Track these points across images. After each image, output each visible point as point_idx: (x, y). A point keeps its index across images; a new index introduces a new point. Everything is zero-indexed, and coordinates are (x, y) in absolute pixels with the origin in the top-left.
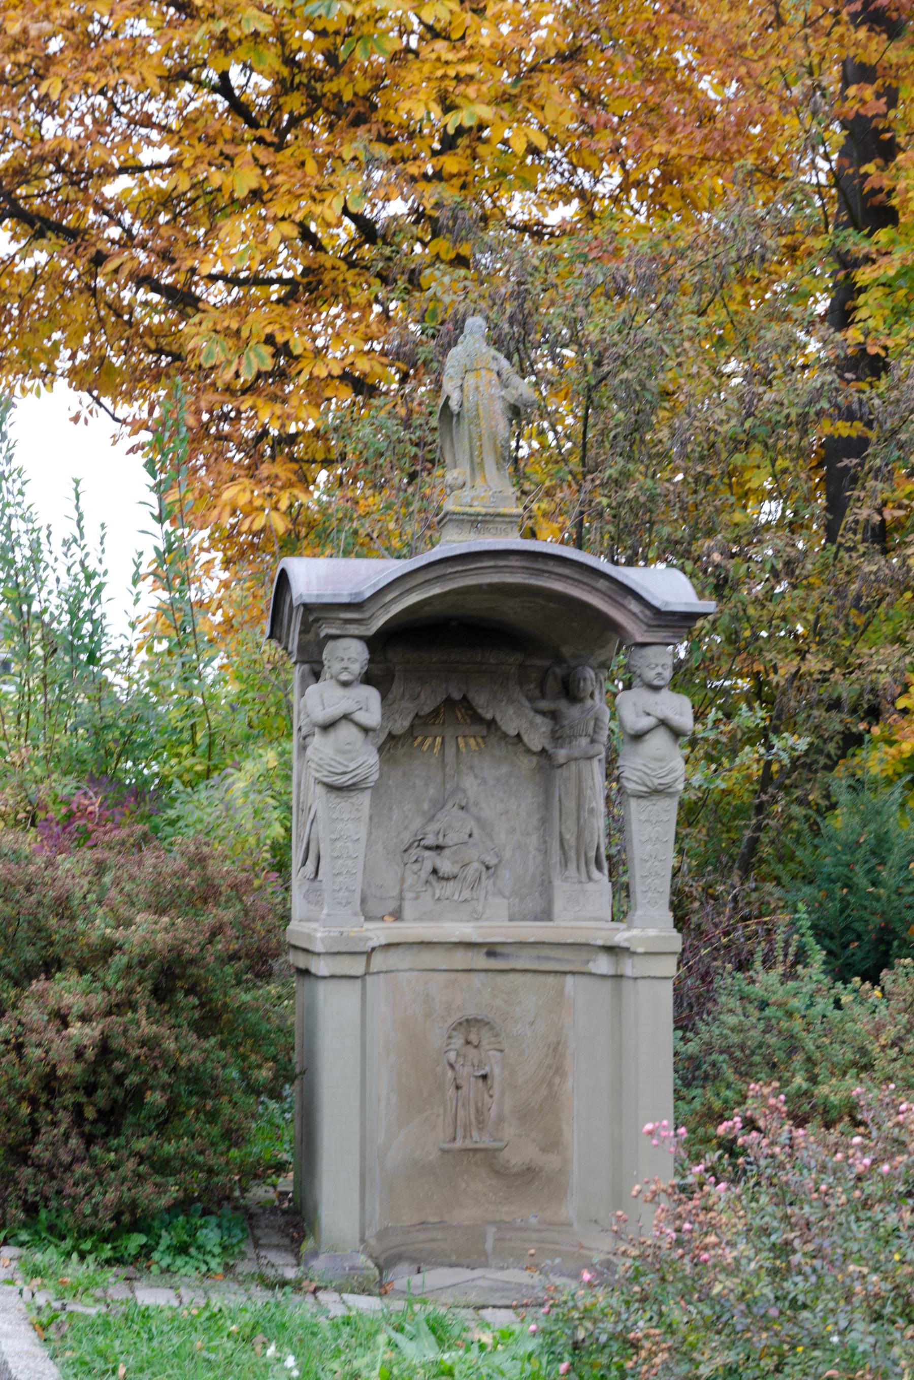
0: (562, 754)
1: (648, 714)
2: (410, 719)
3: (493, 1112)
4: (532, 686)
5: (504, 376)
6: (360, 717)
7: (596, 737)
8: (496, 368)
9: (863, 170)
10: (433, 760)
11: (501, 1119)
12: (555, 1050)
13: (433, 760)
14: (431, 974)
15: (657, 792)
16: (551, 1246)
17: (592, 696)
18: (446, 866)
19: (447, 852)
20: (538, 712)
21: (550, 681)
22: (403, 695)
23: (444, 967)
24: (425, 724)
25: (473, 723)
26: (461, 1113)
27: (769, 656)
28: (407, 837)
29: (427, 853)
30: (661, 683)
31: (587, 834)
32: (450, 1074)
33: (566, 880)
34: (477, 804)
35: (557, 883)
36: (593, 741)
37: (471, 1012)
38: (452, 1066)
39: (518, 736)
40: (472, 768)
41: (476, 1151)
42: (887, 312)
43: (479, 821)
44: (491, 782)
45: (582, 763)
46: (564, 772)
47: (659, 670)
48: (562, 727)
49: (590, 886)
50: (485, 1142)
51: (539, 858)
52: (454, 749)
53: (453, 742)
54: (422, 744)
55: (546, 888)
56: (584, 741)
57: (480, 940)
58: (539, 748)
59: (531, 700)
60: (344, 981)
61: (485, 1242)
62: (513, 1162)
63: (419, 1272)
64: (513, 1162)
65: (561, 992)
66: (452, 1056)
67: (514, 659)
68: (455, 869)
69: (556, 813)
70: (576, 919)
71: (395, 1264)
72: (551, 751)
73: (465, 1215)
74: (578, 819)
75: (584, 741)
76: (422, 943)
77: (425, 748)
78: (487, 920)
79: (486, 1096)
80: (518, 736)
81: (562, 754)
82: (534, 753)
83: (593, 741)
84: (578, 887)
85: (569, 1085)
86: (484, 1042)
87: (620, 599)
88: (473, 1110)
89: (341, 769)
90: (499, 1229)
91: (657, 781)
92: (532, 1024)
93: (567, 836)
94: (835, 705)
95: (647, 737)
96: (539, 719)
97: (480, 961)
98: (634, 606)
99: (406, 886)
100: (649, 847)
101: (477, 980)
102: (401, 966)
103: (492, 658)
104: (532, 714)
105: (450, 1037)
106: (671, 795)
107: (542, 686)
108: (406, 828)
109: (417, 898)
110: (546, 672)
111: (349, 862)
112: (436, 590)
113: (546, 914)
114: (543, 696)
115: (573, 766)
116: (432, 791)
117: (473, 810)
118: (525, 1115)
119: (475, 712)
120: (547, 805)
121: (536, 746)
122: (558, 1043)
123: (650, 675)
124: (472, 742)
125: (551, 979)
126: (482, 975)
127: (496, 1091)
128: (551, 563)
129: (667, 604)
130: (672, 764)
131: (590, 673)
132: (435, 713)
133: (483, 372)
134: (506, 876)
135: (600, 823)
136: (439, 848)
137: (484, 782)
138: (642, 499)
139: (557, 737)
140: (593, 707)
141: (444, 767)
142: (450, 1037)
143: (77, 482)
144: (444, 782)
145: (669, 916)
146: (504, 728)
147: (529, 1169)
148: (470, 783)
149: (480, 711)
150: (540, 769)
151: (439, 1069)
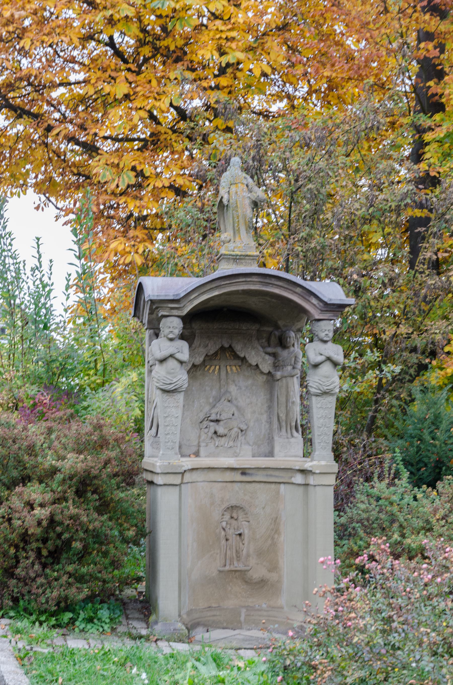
0: (278, 374)
1: (321, 355)
2: (203, 357)
3: (245, 552)
4: (264, 341)
5: (250, 187)
6: (178, 356)
8: (246, 183)
9: (428, 84)
10: (215, 377)
11: (248, 556)
14: (214, 484)
15: (325, 393)
17: (293, 345)
18: (221, 430)
19: (221, 423)
20: (267, 353)
21: (273, 338)
22: (200, 345)
23: (220, 480)
24: (211, 359)
25: (234, 359)
26: (229, 553)
27: (381, 325)
28: (202, 416)
29: (212, 424)
30: (328, 339)
31: (291, 414)
32: (223, 533)
33: (280, 437)
34: (236, 399)
35: (276, 438)
36: (294, 368)
37: (234, 502)
38: (224, 529)
39: (257, 365)
40: (234, 381)
41: (236, 571)
43: (237, 407)
44: (243, 388)
45: (289, 379)
46: (280, 383)
47: (327, 332)
48: (279, 361)
49: (292, 440)
50: (240, 567)
51: (267, 426)
52: (225, 372)
53: (225, 368)
55: (271, 441)
56: (289, 368)
57: (238, 467)
58: (267, 371)
59: (263, 347)
61: (240, 616)
62: (254, 577)
64: (254, 577)
65: (278, 492)
66: (224, 524)
67: (255, 327)
68: (226, 432)
69: (276, 404)
70: (285, 456)
71: (196, 628)
72: (273, 373)
73: (230, 603)
74: (287, 406)
75: (289, 368)
76: (209, 468)
77: (211, 371)
78: (242, 456)
79: (241, 544)
80: (257, 365)
81: (278, 374)
82: (265, 374)
83: (294, 368)
84: (286, 440)
85: (282, 538)
86: (240, 517)
87: (307, 297)
88: (234, 551)
89: (169, 382)
91: (325, 388)
92: (264, 508)
93: (281, 415)
94: (414, 350)
95: (321, 366)
96: (267, 357)
97: (238, 477)
98: (314, 301)
99: (201, 440)
100: (322, 420)
101: (236, 486)
102: (199, 479)
103: (244, 327)
104: (264, 354)
105: (223, 515)
106: (332, 395)
107: (268, 340)
108: (201, 411)
109: (207, 446)
111: (173, 428)
112: (216, 293)
114: (269, 346)
115: (284, 380)
117: (235, 402)
118: (260, 554)
120: (271, 400)
121: (266, 370)
122: (277, 518)
123: (322, 335)
124: (234, 368)
125: (273, 486)
126: (239, 484)
127: (246, 542)
128: (273, 279)
129: (331, 300)
131: (292, 334)
132: (216, 354)
134: (251, 435)
136: (217, 421)
137: (240, 388)
138: (318, 248)
139: (276, 366)
140: (294, 351)
142: (223, 515)
143: (38, 239)
144: (220, 388)
146: (250, 361)
147: (262, 580)
148: (233, 389)
150: (267, 382)
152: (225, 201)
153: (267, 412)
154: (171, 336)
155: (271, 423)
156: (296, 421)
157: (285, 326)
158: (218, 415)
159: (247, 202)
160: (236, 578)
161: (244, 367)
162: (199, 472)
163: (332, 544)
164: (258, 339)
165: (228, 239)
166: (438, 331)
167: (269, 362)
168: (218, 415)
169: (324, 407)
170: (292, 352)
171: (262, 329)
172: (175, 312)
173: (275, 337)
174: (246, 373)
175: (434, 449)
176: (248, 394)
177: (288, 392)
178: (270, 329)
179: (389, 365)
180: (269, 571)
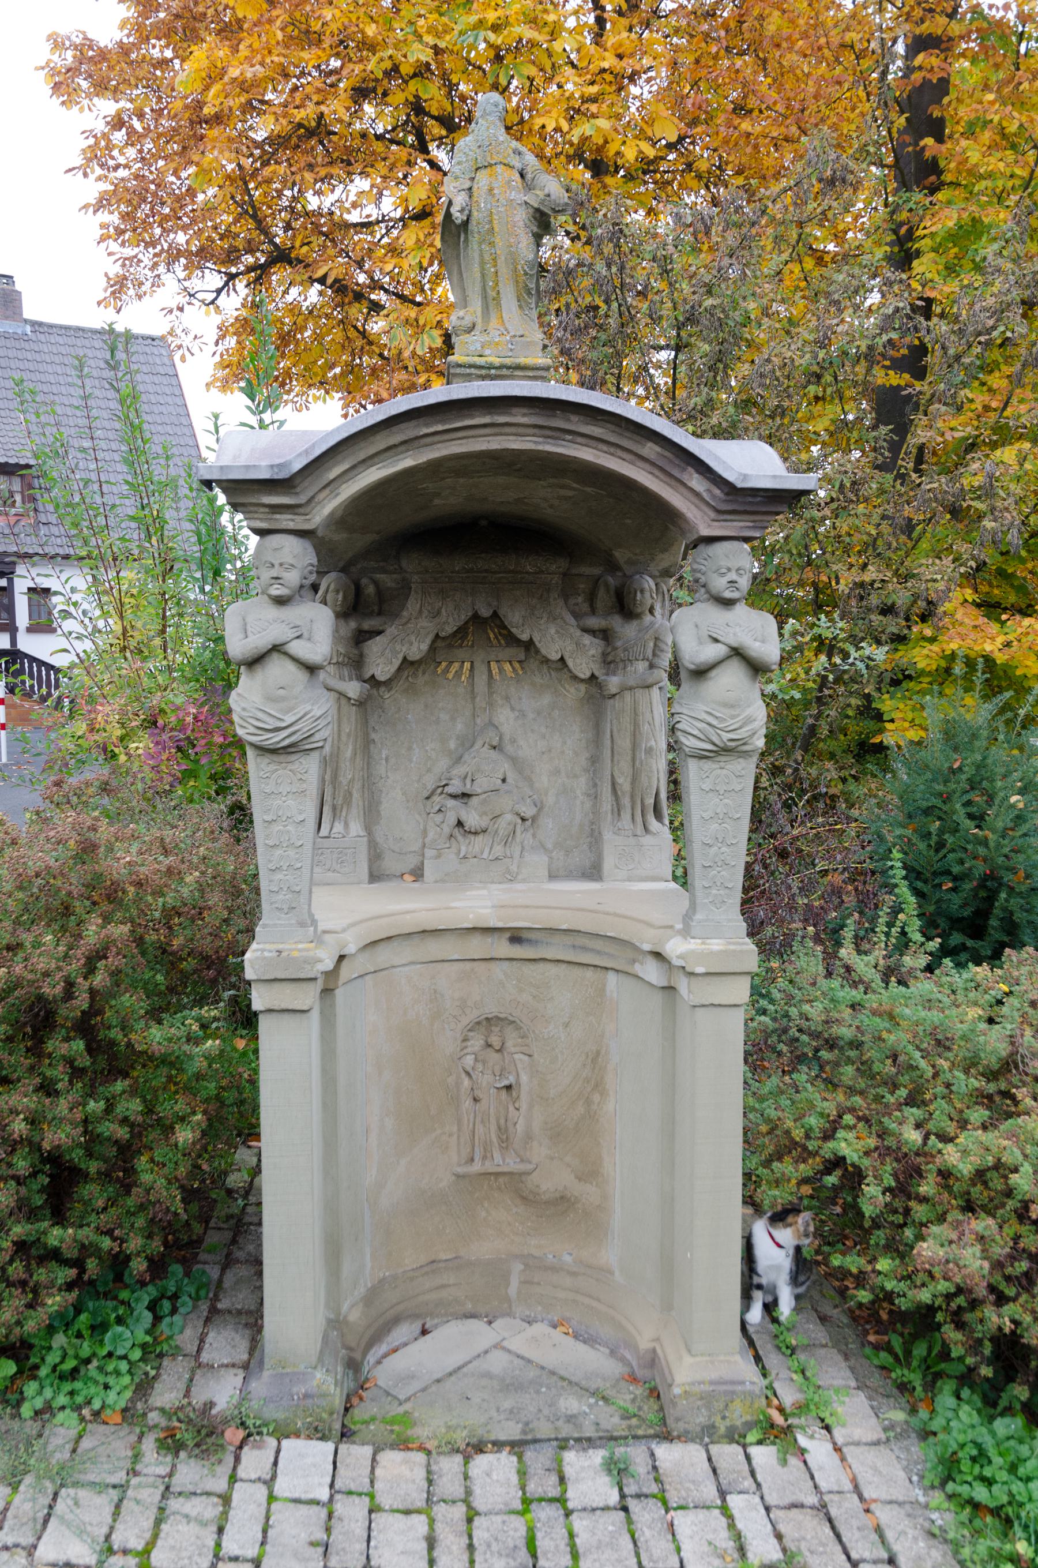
0: (614, 682)
1: (716, 640)
2: (428, 641)
3: (520, 1127)
4: (580, 599)
5: (529, 176)
6: (297, 648)
7: (656, 661)
8: (518, 165)
9: (922, 143)
10: (461, 690)
11: (529, 1137)
12: (594, 1061)
13: (461, 690)
14: (439, 965)
15: (725, 751)
16: (587, 1301)
17: (651, 611)
18: (473, 819)
19: (474, 801)
20: (586, 630)
21: (601, 593)
22: (420, 612)
23: (456, 957)
24: (450, 646)
25: (508, 645)
26: (480, 1129)
27: (835, 567)
28: (430, 782)
29: (451, 803)
30: (736, 595)
31: (644, 779)
32: (466, 1082)
33: (617, 832)
34: (513, 741)
35: (607, 835)
36: (652, 666)
37: (492, 1009)
38: (468, 1074)
39: (562, 659)
40: (507, 698)
41: (497, 1175)
42: (941, 267)
43: (514, 760)
44: (531, 716)
45: (639, 693)
46: (617, 703)
47: (733, 576)
48: (615, 649)
49: (647, 840)
50: (512, 1164)
51: (588, 805)
52: (485, 677)
53: (484, 668)
54: (447, 670)
55: (595, 839)
56: (641, 666)
57: (500, 925)
58: (588, 674)
59: (576, 616)
60: (286, 1016)
61: (508, 1284)
62: (544, 1188)
63: (424, 1332)
64: (544, 1188)
65: (601, 991)
66: (469, 1060)
67: (556, 566)
68: (484, 822)
69: (607, 753)
70: (629, 879)
71: (389, 1331)
72: (602, 678)
73: (484, 1249)
74: (634, 760)
75: (641, 666)
76: (424, 931)
77: (450, 676)
78: (524, 881)
79: (511, 1108)
80: (562, 659)
81: (614, 682)
82: (582, 680)
83: (652, 666)
84: (632, 841)
85: (610, 1106)
86: (509, 1044)
87: (676, 472)
88: (493, 1128)
89: (272, 724)
90: (526, 1265)
91: (726, 736)
92: (566, 1025)
93: (620, 780)
94: (887, 610)
95: (713, 673)
96: (587, 640)
97: (503, 948)
98: (697, 482)
99: (427, 840)
100: (714, 826)
101: (498, 970)
102: (397, 961)
103: (529, 565)
104: (579, 633)
105: (465, 1040)
106: (746, 754)
107: (591, 599)
108: (429, 770)
109: (438, 856)
110: (596, 581)
111: (291, 853)
112: (407, 462)
113: (593, 872)
114: (593, 611)
115: (627, 695)
116: (459, 726)
117: (509, 748)
118: (557, 1134)
119: (505, 628)
120: (597, 741)
121: (584, 674)
122: (598, 1053)
123: (719, 584)
124: (507, 667)
125: (589, 973)
126: (507, 963)
127: (524, 1104)
128: (574, 418)
129: (745, 477)
130: (748, 712)
131: (649, 583)
132: (461, 632)
133: (500, 169)
134: (548, 826)
135: (660, 765)
136: (465, 796)
137: (523, 715)
138: (725, 425)
139: (609, 662)
140: (652, 624)
141: (473, 698)
142: (465, 1040)
143: (216, 417)
144: (474, 716)
145: (741, 926)
146: (543, 651)
147: (562, 1198)
148: (505, 718)
149: (514, 630)
150: (589, 698)
151: (451, 1080)
152: (458, 217)
153: (587, 771)
154: (276, 591)
155: (596, 797)
156: (657, 795)
157: (631, 563)
158: (468, 781)
159: (521, 216)
160: (499, 1189)
161: (533, 664)
162: (395, 943)
163: (741, 1085)
164: (566, 596)
165: (467, 322)
166: (939, 577)
167: (592, 652)
168: (468, 781)
169: (721, 788)
170: (648, 628)
171: (574, 571)
172: (286, 521)
173: (608, 591)
174: (538, 680)
175: (981, 851)
176: (543, 730)
177: (636, 725)
178: (596, 571)
179: (231, 342)
180: (579, 1179)
